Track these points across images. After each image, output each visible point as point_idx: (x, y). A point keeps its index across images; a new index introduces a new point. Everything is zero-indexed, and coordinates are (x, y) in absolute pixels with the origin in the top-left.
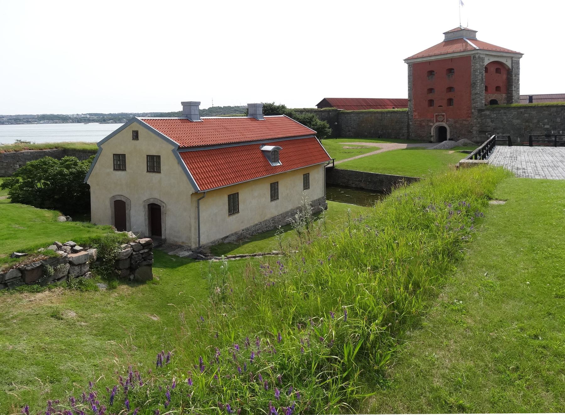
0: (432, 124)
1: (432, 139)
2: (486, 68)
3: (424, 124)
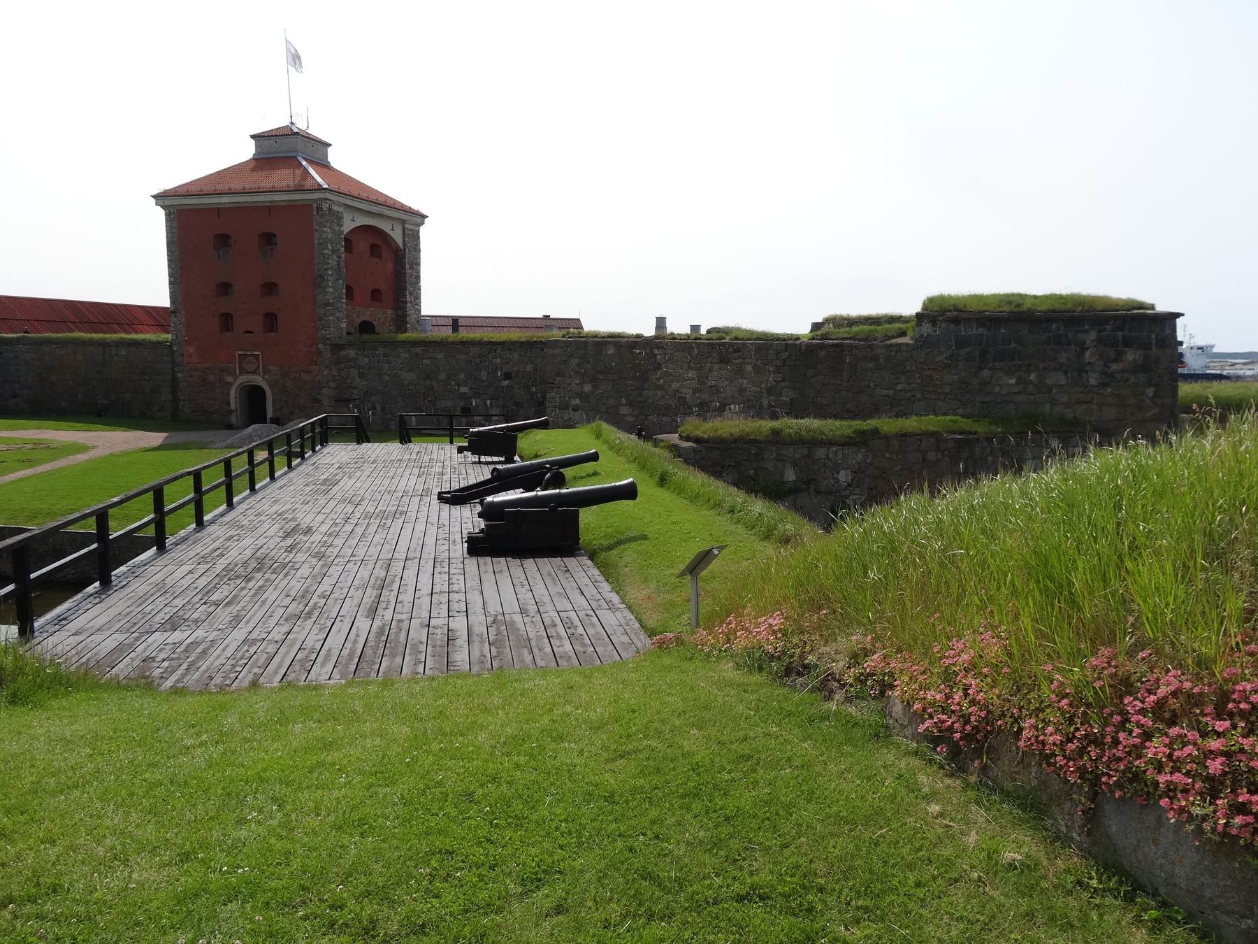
0: (230, 379)
1: (233, 419)
2: (347, 240)
3: (211, 378)
